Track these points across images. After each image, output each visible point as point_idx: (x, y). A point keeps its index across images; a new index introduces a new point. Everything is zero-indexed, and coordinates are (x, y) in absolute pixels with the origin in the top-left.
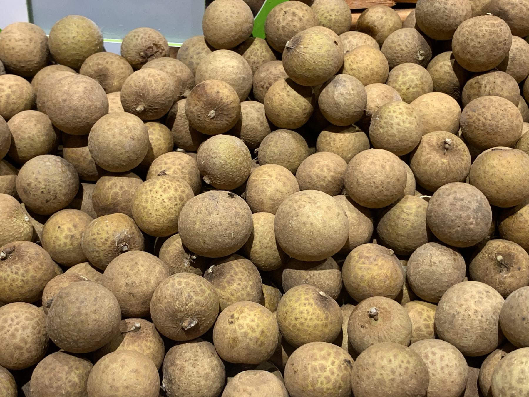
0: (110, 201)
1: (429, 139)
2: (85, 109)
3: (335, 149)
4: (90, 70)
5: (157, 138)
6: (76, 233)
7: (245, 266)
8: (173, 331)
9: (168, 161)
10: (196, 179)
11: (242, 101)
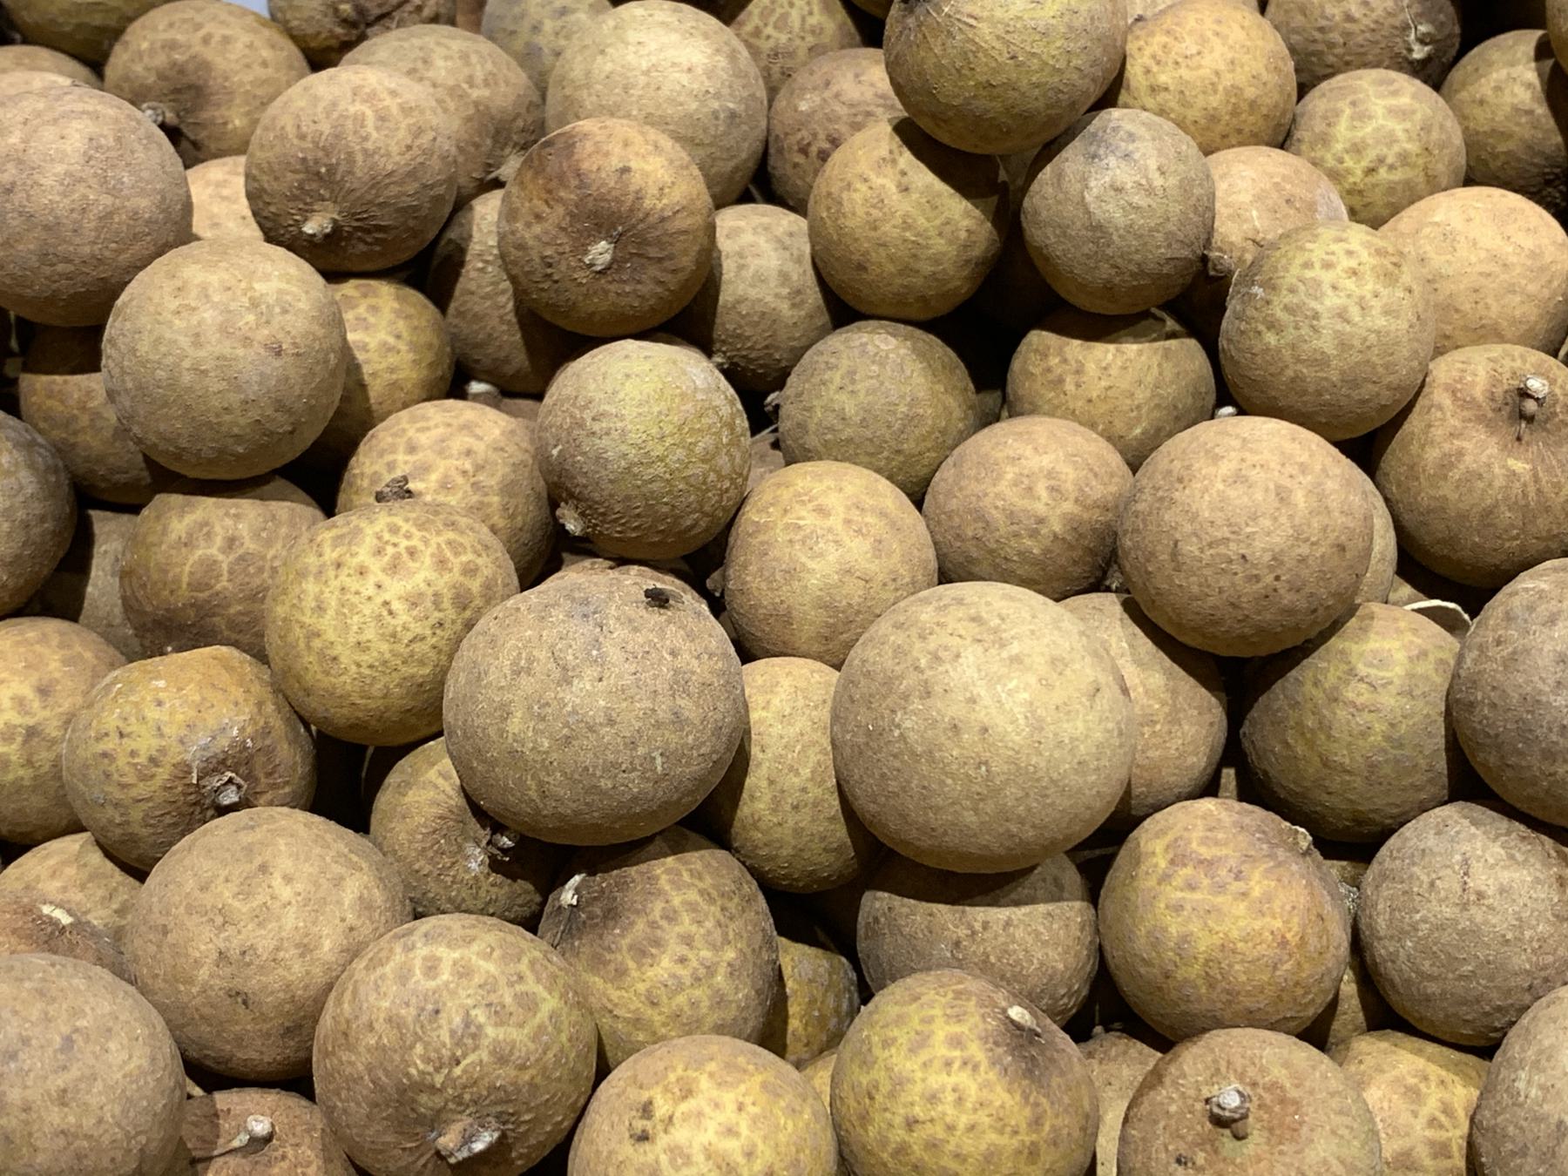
0: (184, 595)
1: (1455, 374)
2: (89, 224)
3: (1079, 405)
4: (138, 68)
5: (385, 343)
6: (45, 716)
7: (709, 880)
8: (402, 1163)
9: (424, 439)
10: (529, 512)
11: (720, 203)
